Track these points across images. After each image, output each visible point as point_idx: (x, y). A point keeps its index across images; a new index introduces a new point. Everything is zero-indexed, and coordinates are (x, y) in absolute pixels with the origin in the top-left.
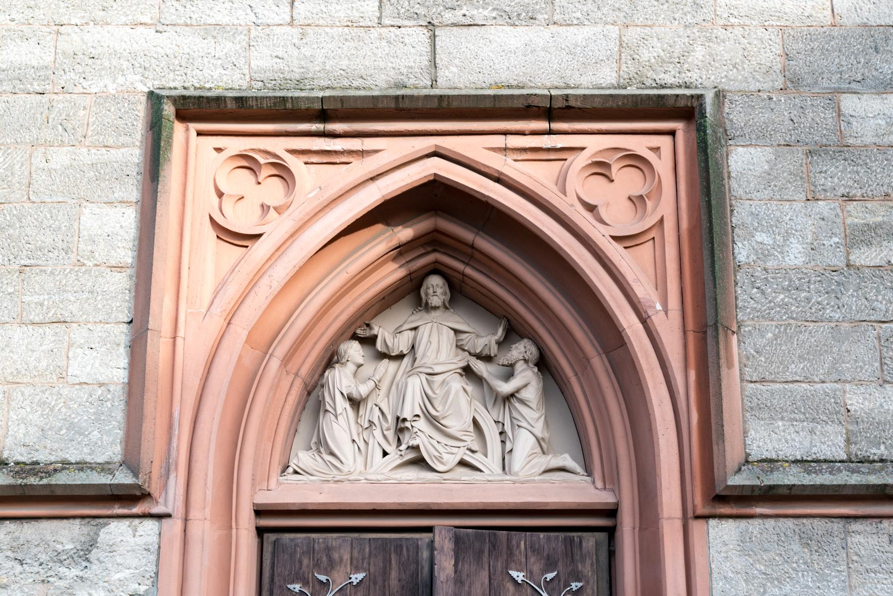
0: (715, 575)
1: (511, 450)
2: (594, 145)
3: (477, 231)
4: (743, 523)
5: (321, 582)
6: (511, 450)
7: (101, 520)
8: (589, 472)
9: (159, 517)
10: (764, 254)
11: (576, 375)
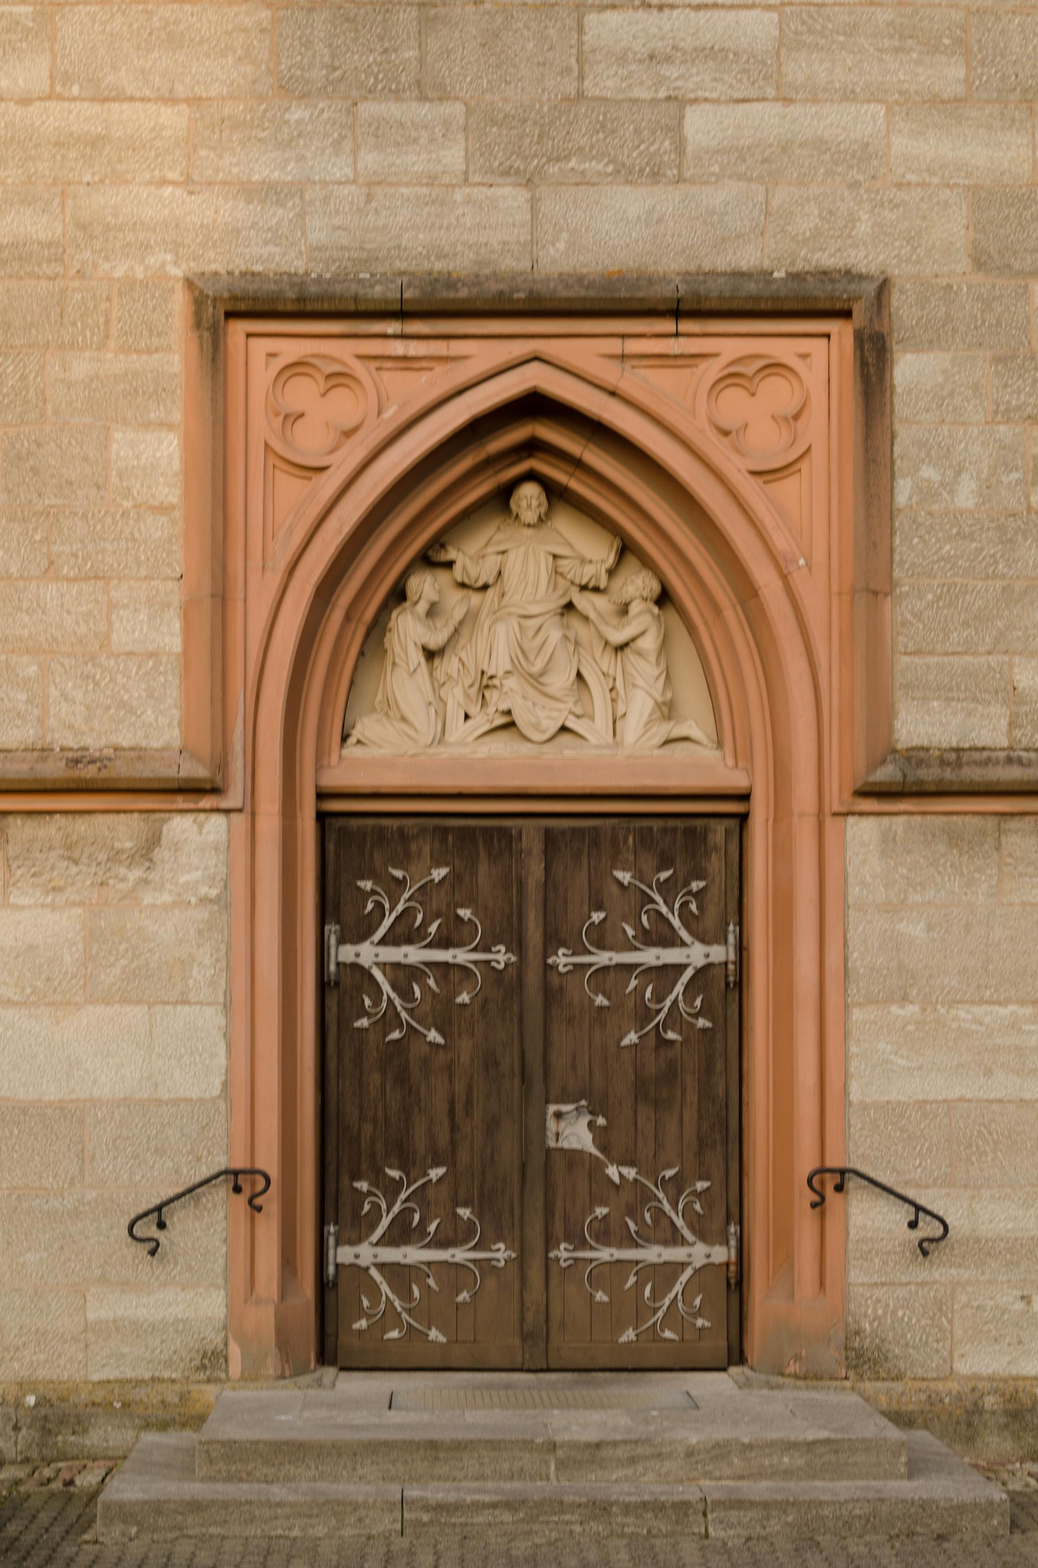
0: (851, 880)
1: (625, 714)
2: (730, 349)
3: (584, 442)
4: (886, 820)
5: (395, 879)
6: (625, 714)
7: (158, 816)
8: (720, 744)
9: (227, 811)
10: (927, 493)
11: (706, 623)
